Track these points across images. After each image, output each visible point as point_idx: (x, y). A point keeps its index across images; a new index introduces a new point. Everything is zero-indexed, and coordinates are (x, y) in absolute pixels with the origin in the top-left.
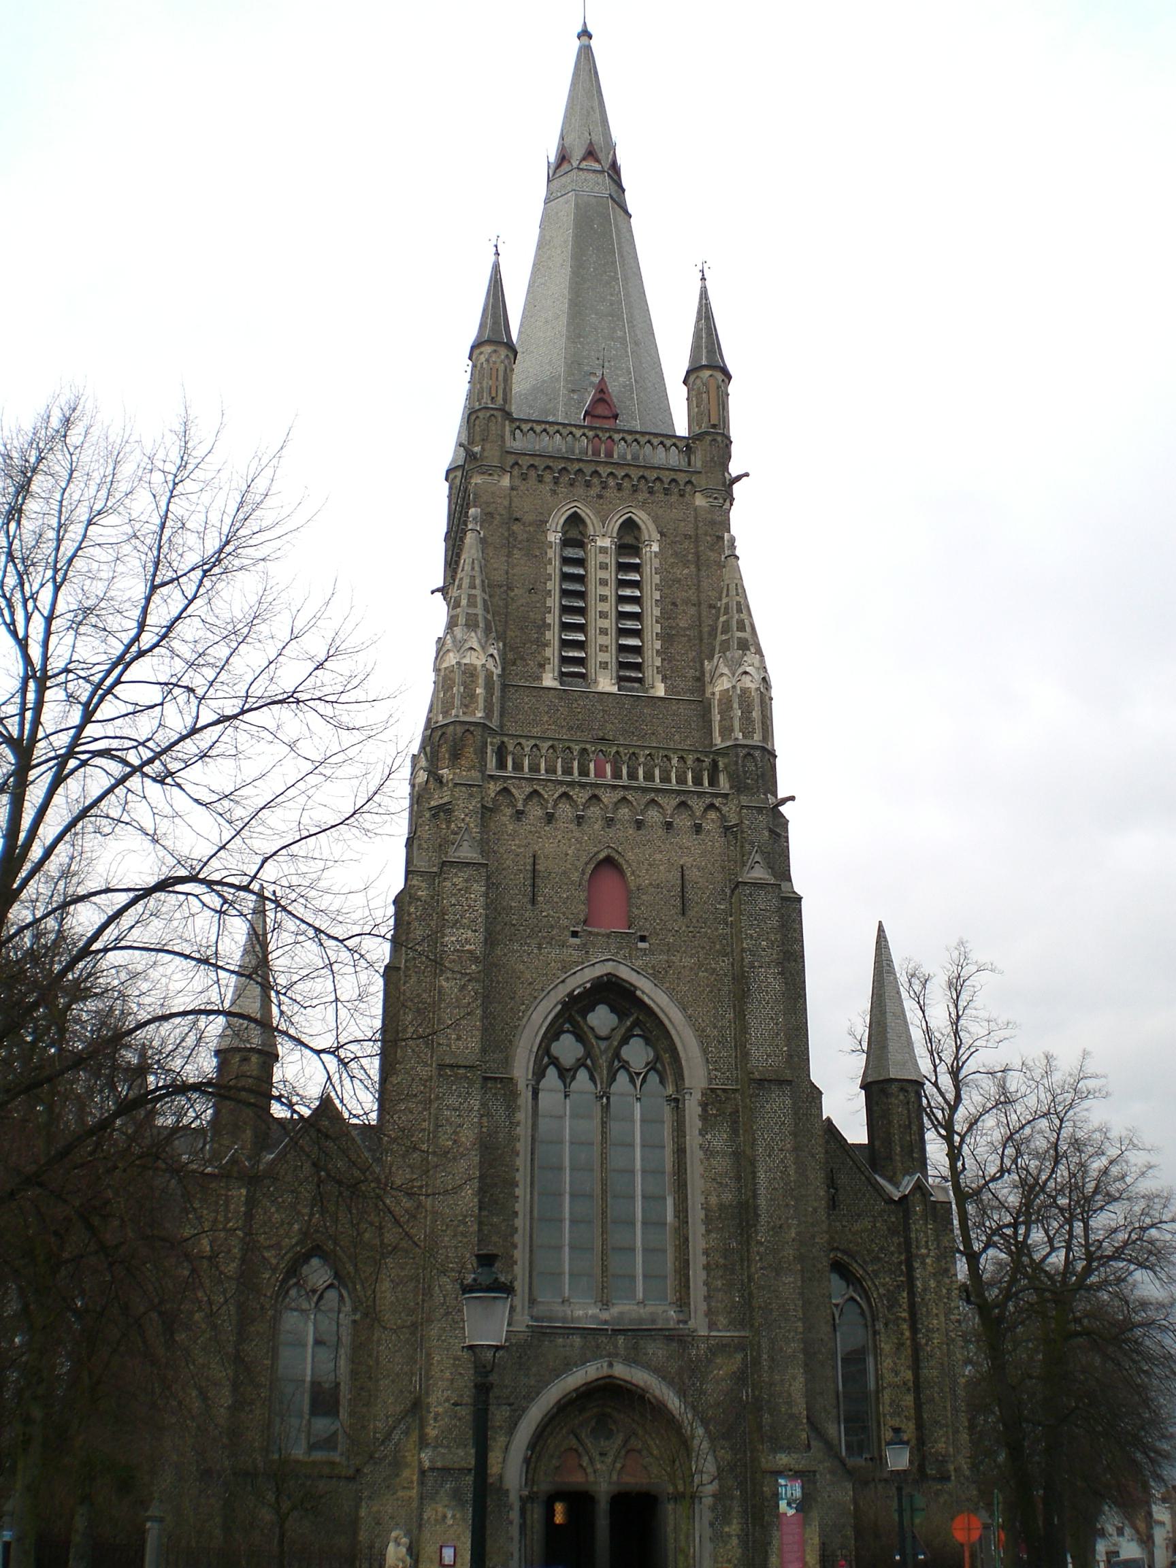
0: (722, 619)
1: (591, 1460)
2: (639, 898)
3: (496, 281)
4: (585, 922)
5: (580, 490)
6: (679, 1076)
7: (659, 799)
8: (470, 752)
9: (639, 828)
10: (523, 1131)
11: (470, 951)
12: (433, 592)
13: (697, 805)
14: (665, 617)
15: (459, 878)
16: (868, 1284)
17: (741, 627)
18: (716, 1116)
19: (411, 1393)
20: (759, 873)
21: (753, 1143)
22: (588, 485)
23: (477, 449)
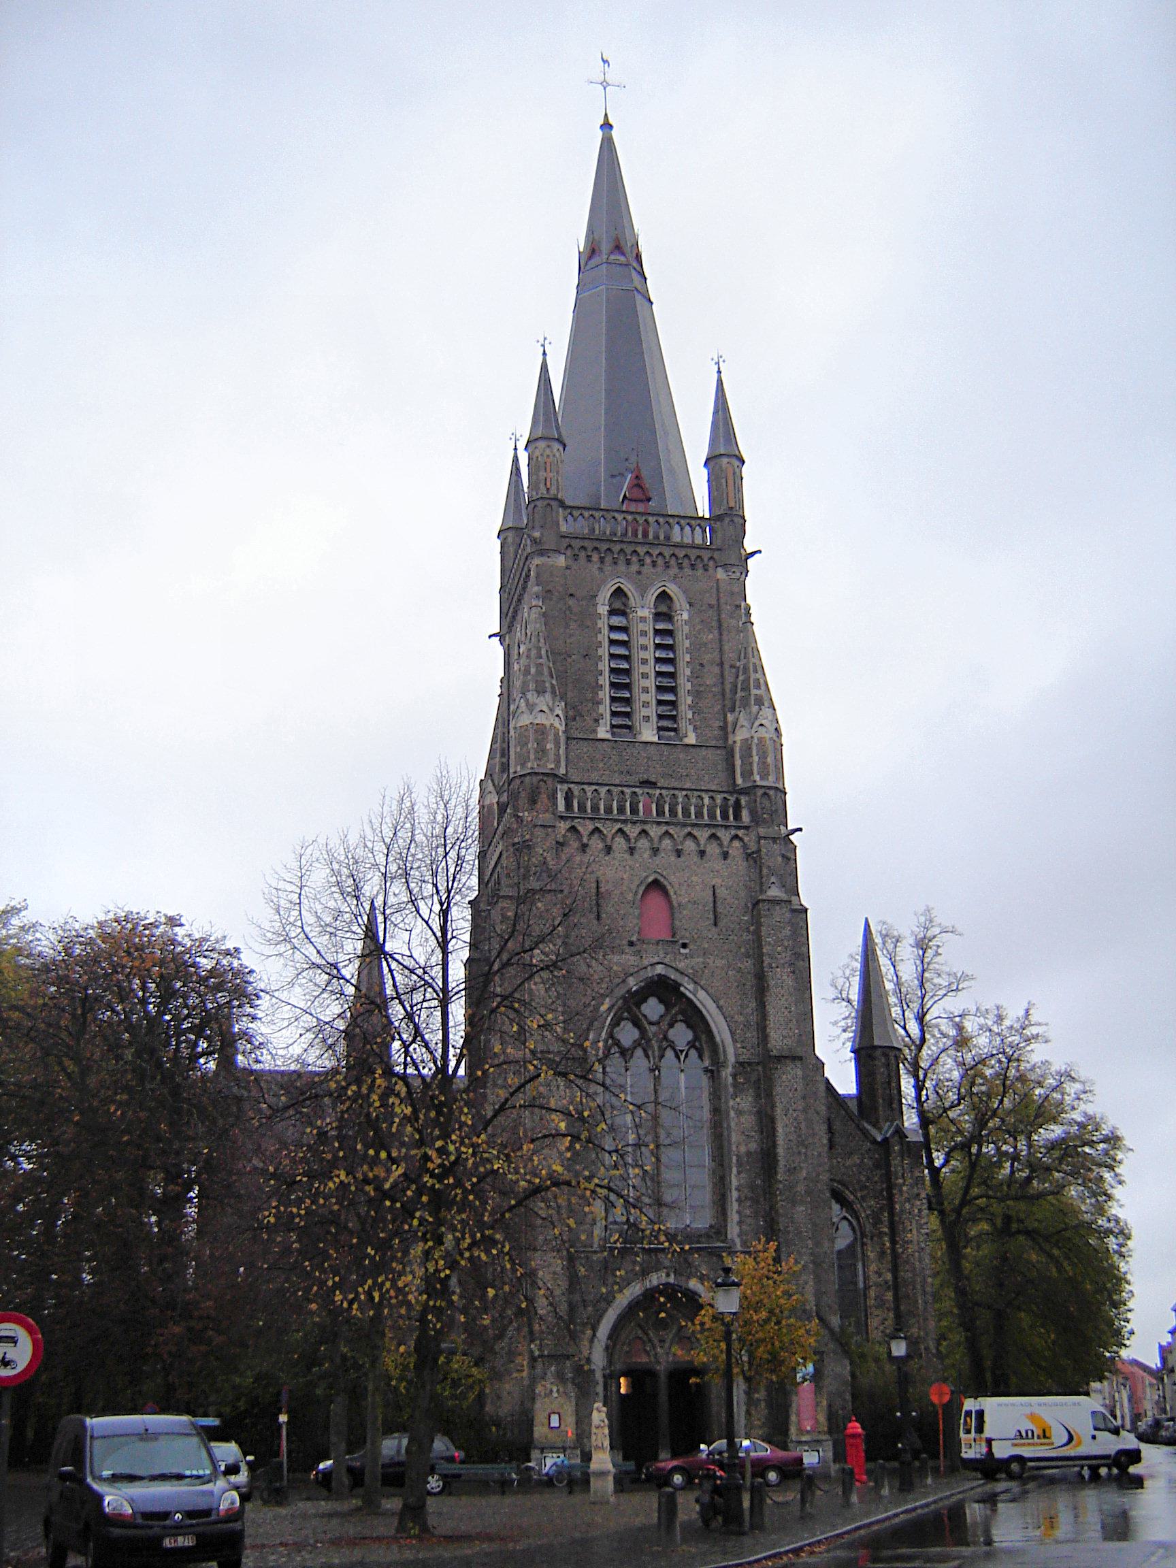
1: (654, 1348)
13: (725, 836)
14: (695, 676)
16: (857, 1206)
20: (774, 892)
21: (773, 1106)
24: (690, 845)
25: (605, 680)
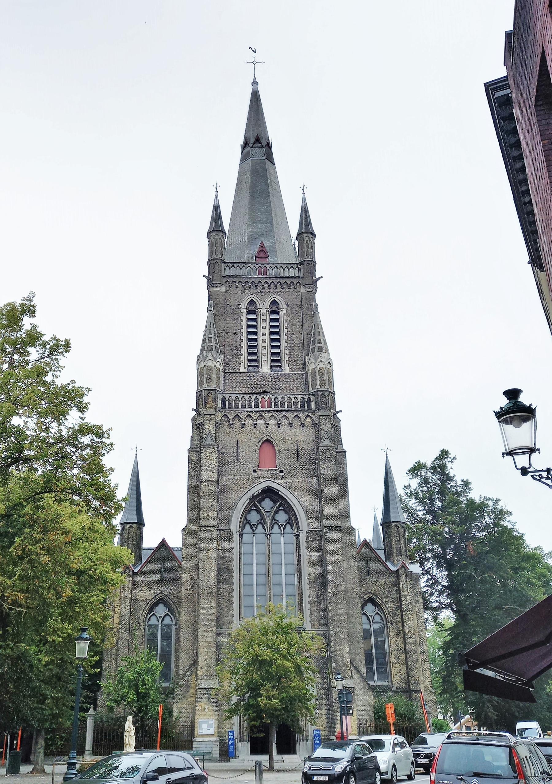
5: (253, 290)
8: (210, 402)
10: (235, 551)
11: (212, 481)
14: (289, 339)
17: (320, 342)
19: (193, 657)
22: (256, 287)
24: (284, 421)
25: (244, 344)
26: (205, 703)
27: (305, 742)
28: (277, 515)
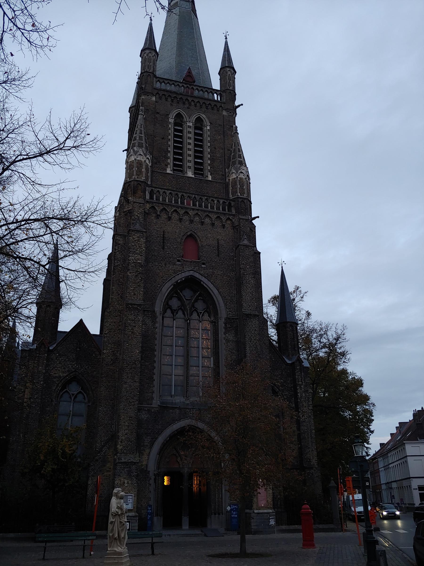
0: (232, 154)
2: (202, 249)
3: (151, 29)
4: (182, 256)
6: (216, 313)
7: (210, 215)
8: (140, 193)
9: (202, 225)
12: (123, 151)
13: (224, 218)
14: (211, 153)
15: (136, 236)
18: (230, 327)
19: (111, 432)
20: (246, 242)
22: (184, 103)
23: (143, 86)
24: (207, 220)
26: (125, 477)
27: (217, 515)
28: (196, 303)
